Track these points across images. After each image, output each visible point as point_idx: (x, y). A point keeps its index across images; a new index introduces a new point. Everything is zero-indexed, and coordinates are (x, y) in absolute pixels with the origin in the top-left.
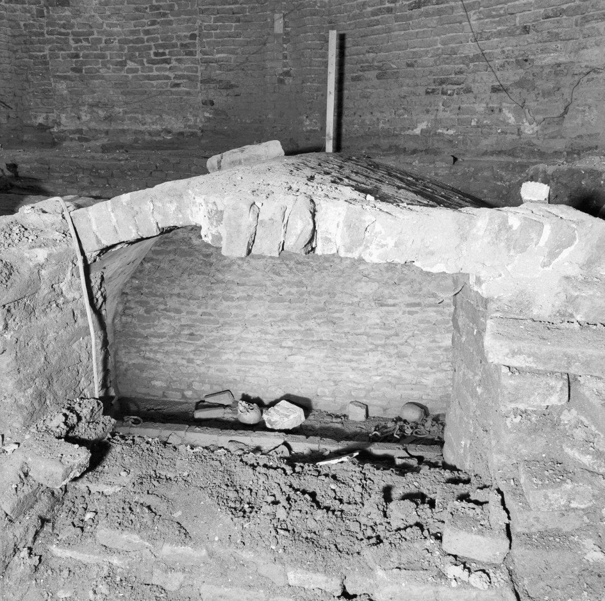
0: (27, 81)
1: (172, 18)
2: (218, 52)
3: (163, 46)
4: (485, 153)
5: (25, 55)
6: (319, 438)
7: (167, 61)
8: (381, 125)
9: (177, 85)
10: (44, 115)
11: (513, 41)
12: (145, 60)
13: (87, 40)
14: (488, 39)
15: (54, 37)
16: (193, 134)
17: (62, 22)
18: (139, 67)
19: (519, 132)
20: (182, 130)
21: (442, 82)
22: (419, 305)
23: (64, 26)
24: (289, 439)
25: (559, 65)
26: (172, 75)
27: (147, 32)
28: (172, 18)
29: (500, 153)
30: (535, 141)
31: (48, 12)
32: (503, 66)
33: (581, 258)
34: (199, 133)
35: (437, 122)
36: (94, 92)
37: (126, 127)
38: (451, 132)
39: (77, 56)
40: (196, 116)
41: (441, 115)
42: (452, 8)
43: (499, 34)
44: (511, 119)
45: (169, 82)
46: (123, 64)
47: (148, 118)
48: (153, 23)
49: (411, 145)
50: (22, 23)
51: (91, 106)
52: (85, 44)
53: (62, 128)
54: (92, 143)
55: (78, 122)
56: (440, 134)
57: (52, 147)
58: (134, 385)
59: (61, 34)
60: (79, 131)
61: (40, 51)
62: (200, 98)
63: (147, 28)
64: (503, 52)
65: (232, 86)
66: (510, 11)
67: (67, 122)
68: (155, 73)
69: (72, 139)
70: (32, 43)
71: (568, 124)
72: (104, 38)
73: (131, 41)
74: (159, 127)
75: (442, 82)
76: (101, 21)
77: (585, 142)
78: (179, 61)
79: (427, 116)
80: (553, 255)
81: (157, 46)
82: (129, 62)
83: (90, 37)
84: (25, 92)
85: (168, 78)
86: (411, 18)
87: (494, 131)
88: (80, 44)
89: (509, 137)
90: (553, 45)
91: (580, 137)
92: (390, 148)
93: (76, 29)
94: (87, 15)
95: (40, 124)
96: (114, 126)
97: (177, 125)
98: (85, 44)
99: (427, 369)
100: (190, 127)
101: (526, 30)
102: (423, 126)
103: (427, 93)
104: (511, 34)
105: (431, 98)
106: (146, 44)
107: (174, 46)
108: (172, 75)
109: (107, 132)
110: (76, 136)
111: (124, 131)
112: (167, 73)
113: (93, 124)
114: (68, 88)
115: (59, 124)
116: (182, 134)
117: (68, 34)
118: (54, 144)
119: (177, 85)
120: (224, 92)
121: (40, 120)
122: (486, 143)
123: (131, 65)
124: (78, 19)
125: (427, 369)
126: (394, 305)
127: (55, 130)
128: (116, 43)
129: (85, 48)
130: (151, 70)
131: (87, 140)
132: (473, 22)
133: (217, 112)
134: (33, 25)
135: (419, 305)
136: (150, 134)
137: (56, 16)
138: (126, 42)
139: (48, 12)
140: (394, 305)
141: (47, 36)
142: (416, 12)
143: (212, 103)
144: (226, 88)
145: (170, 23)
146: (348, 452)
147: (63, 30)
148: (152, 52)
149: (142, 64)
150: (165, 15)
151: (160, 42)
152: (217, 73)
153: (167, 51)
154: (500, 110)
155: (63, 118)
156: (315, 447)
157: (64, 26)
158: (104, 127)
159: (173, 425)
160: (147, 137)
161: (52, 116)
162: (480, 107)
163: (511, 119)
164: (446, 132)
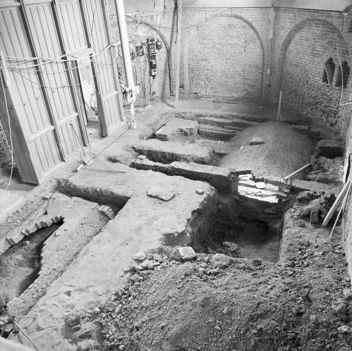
6: (97, 204)
18: (225, 79)
23: (204, 67)
24: (261, 190)
26: (235, 81)
28: (236, 66)
34: (242, 98)
37: (220, 95)
39: (207, 75)
41: (309, 111)
48: (230, 67)
50: (192, 65)
58: (345, 250)
68: (230, 81)
78: (237, 78)
93: (207, 68)
96: (216, 95)
108: (235, 81)
110: (206, 97)
115: (200, 93)
118: (198, 98)
121: (195, 92)
123: (223, 78)
128: (219, 72)
131: (208, 98)
145: (235, 67)
146: (274, 195)
147: (204, 68)
150: (234, 65)
151: (232, 72)
155: (202, 92)
156: (267, 193)
157: (204, 67)
159: (209, 173)
160: (226, 98)
161: (199, 90)
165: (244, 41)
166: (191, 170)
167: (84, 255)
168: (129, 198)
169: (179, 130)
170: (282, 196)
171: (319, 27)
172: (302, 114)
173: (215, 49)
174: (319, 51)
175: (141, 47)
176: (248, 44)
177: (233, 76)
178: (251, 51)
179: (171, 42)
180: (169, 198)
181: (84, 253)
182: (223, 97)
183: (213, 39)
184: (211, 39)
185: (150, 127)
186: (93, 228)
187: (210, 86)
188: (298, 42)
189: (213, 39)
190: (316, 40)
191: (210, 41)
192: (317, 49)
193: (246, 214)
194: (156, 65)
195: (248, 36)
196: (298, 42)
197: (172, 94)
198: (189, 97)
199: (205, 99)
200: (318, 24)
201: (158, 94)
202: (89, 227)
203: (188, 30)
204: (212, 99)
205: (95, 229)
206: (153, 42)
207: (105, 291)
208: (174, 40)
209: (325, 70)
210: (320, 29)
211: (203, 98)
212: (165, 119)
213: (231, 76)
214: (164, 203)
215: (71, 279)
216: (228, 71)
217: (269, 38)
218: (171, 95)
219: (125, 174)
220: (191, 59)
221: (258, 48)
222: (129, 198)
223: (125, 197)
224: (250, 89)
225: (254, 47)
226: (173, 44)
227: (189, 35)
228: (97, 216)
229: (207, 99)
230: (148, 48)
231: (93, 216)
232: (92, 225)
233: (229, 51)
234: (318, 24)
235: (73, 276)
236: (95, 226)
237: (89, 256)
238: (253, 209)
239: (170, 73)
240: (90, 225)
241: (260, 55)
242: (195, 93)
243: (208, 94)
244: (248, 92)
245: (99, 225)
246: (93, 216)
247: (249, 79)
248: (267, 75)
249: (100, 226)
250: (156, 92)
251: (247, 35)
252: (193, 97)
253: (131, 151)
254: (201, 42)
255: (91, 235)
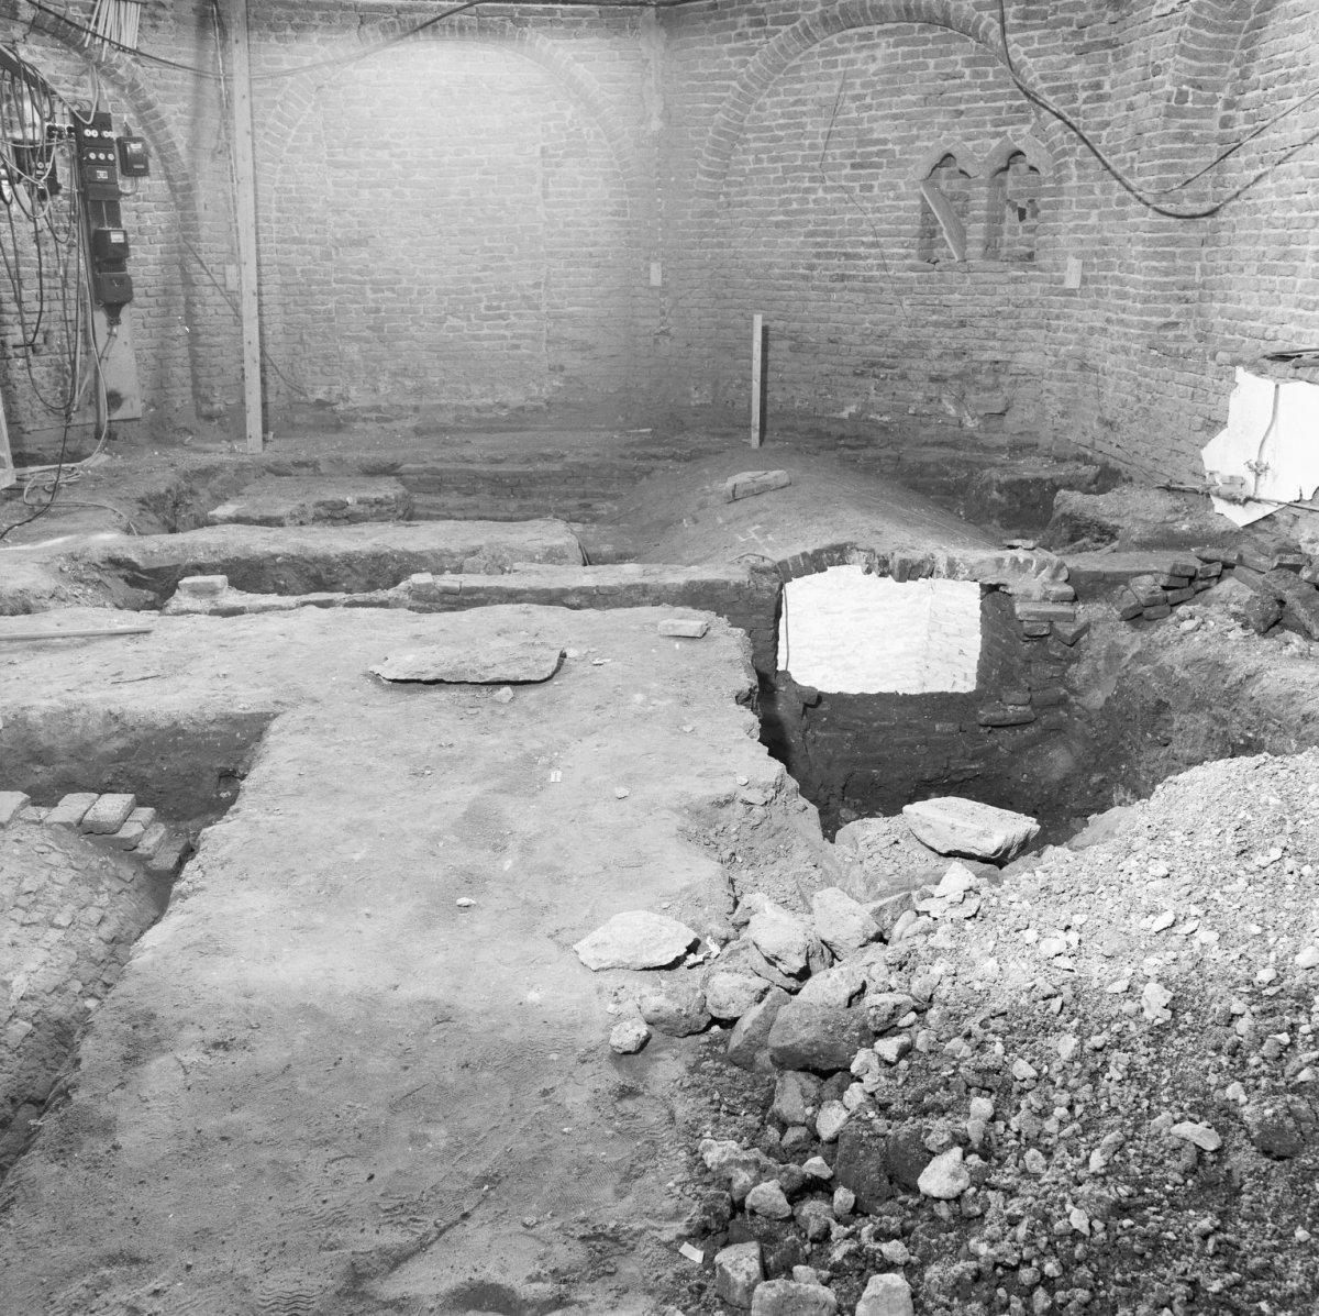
0: (301, 342)
1: (511, 263)
2: (571, 305)
3: (496, 297)
4: (925, 444)
5: (300, 309)
7: (501, 317)
8: (797, 404)
9: (517, 347)
10: (326, 388)
11: (949, 333)
12: (472, 315)
13: (393, 290)
14: (923, 326)
15: (344, 286)
16: (537, 409)
17: (355, 267)
18: (465, 324)
19: (961, 425)
20: (521, 404)
21: (873, 365)
22: (867, 610)
23: (360, 273)
25: (997, 362)
26: (508, 333)
27: (477, 280)
28: (511, 263)
29: (941, 444)
30: (977, 435)
31: (337, 254)
32: (940, 357)
33: (1050, 574)
34: (546, 408)
35: (868, 406)
36: (398, 356)
38: (886, 418)
39: (377, 310)
40: (541, 385)
41: (872, 398)
42: (882, 290)
43: (936, 324)
44: (952, 412)
45: (505, 343)
46: (441, 321)
47: (476, 390)
48: (484, 269)
49: (836, 429)
50: (298, 269)
51: (395, 374)
52: (388, 294)
53: (350, 404)
54: (397, 425)
55: (374, 397)
56: (872, 421)
57: (336, 432)
59: (355, 282)
60: (377, 409)
61: (323, 304)
62: (546, 362)
63: (476, 274)
64: (940, 343)
65: (590, 348)
66: (945, 303)
67: (359, 397)
68: (486, 331)
69: (365, 420)
70: (312, 294)
71: (1009, 421)
72: (417, 287)
73: (453, 291)
74: (490, 401)
75: (873, 365)
76: (412, 266)
77: (1026, 439)
78: (520, 316)
79: (858, 399)
80: (1038, 573)
81: (489, 299)
82: (449, 317)
83: (396, 287)
84: (298, 359)
85: (504, 337)
86: (832, 290)
87: (934, 421)
88: (381, 295)
89: (950, 429)
90: (991, 344)
91: (1021, 434)
92: (811, 431)
93: (376, 276)
94: (393, 258)
95: (318, 400)
96: (425, 402)
97: (515, 398)
98: (388, 294)
99: (876, 680)
100: (532, 399)
101: (962, 324)
102: (852, 409)
103: (855, 374)
104: (948, 326)
105: (862, 381)
106: (475, 295)
107: (512, 297)
109: (416, 409)
110: (374, 415)
111: (440, 408)
112: (502, 332)
113: (396, 399)
114: (361, 350)
115: (346, 400)
116: (522, 408)
117: (365, 283)
118: (338, 428)
119: (517, 347)
120: (579, 355)
121: (320, 395)
122: (924, 433)
123: (452, 321)
124: (381, 263)
125: (876, 680)
126: (840, 613)
127: (341, 407)
128: (433, 294)
129: (388, 299)
130: (481, 328)
131: (388, 420)
132: (905, 307)
133: (568, 380)
134: (316, 272)
135: (867, 610)
136: (478, 410)
137: (349, 259)
138: (446, 293)
139: (337, 254)
140: (840, 613)
141: (334, 285)
142: (839, 285)
143: (562, 368)
144: (582, 350)
145: (507, 269)
147: (359, 278)
148: (482, 305)
149: (469, 319)
151: (494, 292)
152: (570, 332)
153: (503, 304)
154: (940, 401)
155: (353, 393)
157: (360, 273)
158: (412, 401)
160: (475, 414)
161: (337, 390)
162: (919, 396)
163: (952, 412)
164: (878, 418)
165: (537, 154)
166: (546, 586)
167: (130, 1060)
168: (267, 718)
169: (321, 510)
170: (1050, 614)
171: (876, 46)
172: (841, 421)
173: (407, 191)
174: (885, 142)
175: (46, 154)
176: (558, 165)
177: (499, 308)
178: (572, 194)
179: (194, 146)
180: (554, 664)
181: (116, 1049)
182: (457, 408)
183: (398, 146)
184: (386, 145)
185: (155, 511)
186: (54, 935)
187: (391, 365)
188: (782, 127)
189: (398, 146)
190: (868, 100)
191: (384, 155)
192: (875, 136)
193: (879, 762)
194: (124, 246)
195: (553, 131)
196: (782, 127)
197: (205, 408)
198: (293, 426)
199: (370, 426)
200: (868, 36)
201: (133, 407)
202: (15, 929)
203: (278, 98)
204: (409, 424)
205: (74, 938)
206: (106, 134)
207: (569, 1255)
208: (208, 141)
209: (926, 211)
210: (879, 53)
211: (358, 426)
212: (208, 495)
213: (488, 308)
214: (532, 694)
215: (106, 1284)
216: (474, 286)
217: (648, 133)
218: (199, 414)
219: (152, 636)
220: (295, 241)
221: (601, 179)
222: (267, 718)
223: (235, 722)
224: (574, 362)
225: (581, 178)
226: (206, 164)
227: (280, 118)
228: (55, 858)
229: (385, 425)
230: (82, 166)
231: (22, 858)
232: (36, 916)
233: (473, 196)
234: (868, 36)
235: (112, 1244)
236: (62, 920)
237: (193, 1056)
238: (908, 726)
239: (189, 304)
240: (19, 915)
241: (609, 209)
242: (320, 404)
243: (384, 404)
244: (568, 380)
245: (93, 914)
246: (22, 858)
247: (570, 316)
248: (652, 289)
249: (103, 919)
250: (124, 390)
251: (551, 124)
252: (311, 422)
253: (108, 581)
254: (340, 158)
255: (55, 981)
